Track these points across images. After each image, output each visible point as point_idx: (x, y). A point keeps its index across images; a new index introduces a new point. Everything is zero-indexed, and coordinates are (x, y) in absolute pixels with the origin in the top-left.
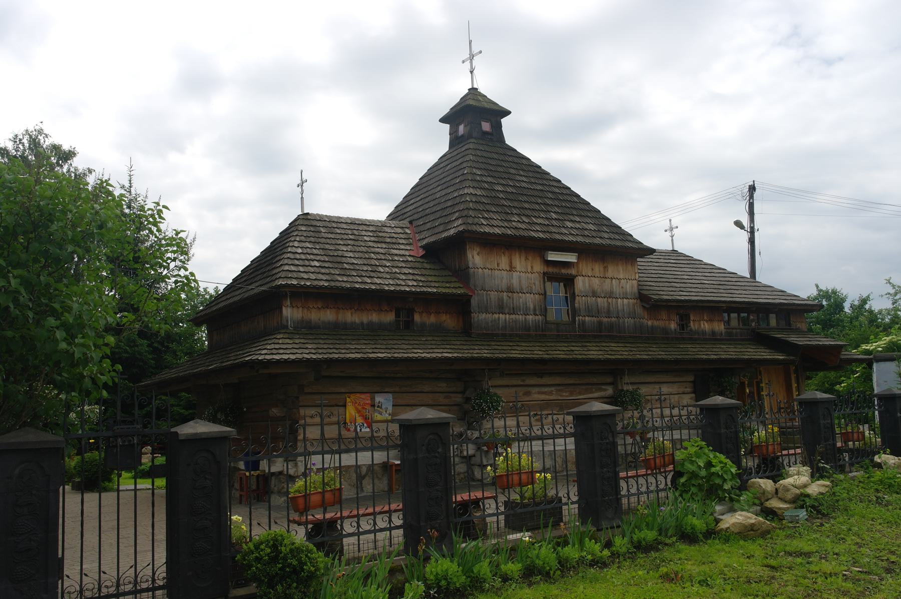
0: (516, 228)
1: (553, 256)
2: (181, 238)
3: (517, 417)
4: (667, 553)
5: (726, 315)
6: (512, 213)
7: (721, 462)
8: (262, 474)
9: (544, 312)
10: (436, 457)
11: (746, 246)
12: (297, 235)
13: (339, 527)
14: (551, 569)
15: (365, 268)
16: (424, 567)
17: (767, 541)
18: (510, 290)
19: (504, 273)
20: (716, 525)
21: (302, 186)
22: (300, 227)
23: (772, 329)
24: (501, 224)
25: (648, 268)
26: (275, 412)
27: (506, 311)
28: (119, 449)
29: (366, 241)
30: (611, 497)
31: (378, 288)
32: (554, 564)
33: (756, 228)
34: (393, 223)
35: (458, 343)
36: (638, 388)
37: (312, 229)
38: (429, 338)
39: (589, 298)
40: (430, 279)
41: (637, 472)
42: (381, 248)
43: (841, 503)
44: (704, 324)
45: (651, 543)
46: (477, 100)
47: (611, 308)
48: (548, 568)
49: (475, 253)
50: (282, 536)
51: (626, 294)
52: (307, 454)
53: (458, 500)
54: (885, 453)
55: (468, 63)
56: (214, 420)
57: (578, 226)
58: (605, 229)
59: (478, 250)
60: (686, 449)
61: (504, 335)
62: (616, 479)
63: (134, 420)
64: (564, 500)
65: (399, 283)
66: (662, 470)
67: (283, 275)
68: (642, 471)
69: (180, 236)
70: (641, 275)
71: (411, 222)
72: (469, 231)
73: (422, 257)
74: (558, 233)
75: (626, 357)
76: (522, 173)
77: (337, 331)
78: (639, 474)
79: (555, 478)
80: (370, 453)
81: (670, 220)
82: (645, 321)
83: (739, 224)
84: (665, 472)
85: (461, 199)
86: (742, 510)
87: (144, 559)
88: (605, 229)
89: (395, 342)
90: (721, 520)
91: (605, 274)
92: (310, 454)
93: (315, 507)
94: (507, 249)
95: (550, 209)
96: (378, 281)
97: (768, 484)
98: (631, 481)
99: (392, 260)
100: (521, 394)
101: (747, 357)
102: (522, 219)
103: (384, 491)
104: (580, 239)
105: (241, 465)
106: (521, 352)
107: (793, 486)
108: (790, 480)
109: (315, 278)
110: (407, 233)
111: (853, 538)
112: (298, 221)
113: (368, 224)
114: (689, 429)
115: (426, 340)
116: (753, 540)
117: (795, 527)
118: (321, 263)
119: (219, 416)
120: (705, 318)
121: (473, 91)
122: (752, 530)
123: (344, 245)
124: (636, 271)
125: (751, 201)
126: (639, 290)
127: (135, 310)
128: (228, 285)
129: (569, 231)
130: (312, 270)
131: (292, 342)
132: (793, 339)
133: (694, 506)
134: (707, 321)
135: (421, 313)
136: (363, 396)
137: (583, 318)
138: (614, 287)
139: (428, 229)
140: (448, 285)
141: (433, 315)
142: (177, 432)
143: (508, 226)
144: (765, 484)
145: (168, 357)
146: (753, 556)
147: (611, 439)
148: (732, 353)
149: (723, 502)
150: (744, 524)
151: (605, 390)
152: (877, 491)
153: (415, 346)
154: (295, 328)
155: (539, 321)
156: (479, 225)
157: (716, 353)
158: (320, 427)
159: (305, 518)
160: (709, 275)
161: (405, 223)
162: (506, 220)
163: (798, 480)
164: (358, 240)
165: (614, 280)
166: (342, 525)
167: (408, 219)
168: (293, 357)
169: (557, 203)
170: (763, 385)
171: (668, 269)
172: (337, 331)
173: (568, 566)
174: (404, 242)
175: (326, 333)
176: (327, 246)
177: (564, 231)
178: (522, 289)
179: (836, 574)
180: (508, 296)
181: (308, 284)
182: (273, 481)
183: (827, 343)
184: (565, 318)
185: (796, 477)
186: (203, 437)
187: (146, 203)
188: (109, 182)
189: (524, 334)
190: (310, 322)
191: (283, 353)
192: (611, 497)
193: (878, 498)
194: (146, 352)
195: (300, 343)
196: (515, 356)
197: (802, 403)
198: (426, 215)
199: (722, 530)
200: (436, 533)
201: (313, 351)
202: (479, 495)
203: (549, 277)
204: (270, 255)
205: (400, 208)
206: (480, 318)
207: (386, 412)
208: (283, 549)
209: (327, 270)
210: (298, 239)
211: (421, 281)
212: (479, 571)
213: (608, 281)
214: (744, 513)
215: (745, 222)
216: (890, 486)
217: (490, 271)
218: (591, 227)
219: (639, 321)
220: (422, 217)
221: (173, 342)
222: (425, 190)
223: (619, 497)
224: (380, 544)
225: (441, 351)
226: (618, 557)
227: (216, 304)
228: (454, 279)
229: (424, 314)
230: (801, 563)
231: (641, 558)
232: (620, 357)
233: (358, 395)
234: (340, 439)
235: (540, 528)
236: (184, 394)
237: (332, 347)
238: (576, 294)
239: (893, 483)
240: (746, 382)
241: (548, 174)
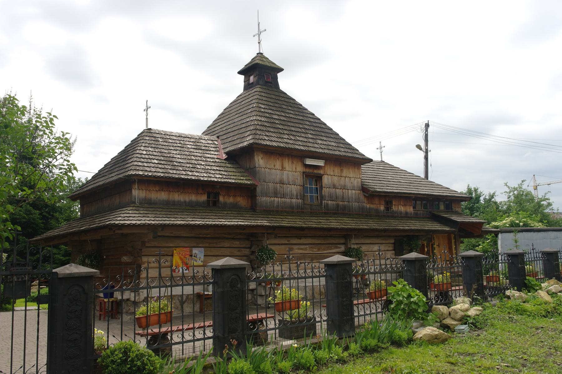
0: (286, 143)
1: (309, 162)
2: (66, 139)
4: (384, 354)
6: (284, 133)
7: (417, 295)
8: (115, 300)
10: (236, 290)
11: (423, 160)
12: (143, 143)
13: (169, 338)
14: (310, 366)
15: (188, 165)
16: (227, 365)
17: (446, 346)
18: (282, 182)
19: (278, 172)
20: (413, 335)
21: (147, 110)
22: (145, 137)
23: (442, 211)
24: (276, 139)
25: (367, 171)
26: (125, 259)
27: (279, 196)
28: (14, 284)
29: (188, 148)
30: (348, 317)
32: (313, 362)
33: (429, 149)
34: (206, 137)
35: (248, 215)
36: (361, 247)
37: (153, 139)
40: (230, 174)
41: (364, 301)
42: (199, 153)
43: (489, 321)
45: (374, 347)
46: (262, 61)
48: (309, 365)
49: (260, 158)
50: (130, 345)
51: (354, 187)
52: (148, 287)
53: (249, 319)
54: (514, 290)
55: (257, 37)
56: (83, 264)
57: (325, 143)
58: (342, 145)
59: (262, 156)
60: (395, 286)
61: (277, 211)
62: (351, 305)
63: (26, 264)
64: (318, 319)
65: (210, 176)
66: (379, 299)
67: (133, 168)
68: (367, 300)
69: (65, 137)
70: (363, 175)
71: (218, 137)
72: (256, 144)
74: (313, 147)
75: (354, 227)
76: (290, 108)
78: (365, 302)
79: (313, 304)
81: (380, 142)
82: (365, 205)
83: (419, 147)
84: (381, 300)
85: (251, 123)
86: (430, 325)
88: (342, 145)
89: (207, 214)
90: (417, 332)
91: (341, 174)
92: (151, 288)
93: (153, 325)
94: (281, 156)
95: (307, 131)
96: (197, 174)
97: (445, 309)
98: (360, 306)
99: (206, 161)
101: (427, 228)
102: (290, 137)
103: (197, 312)
104: (326, 151)
105: (102, 295)
106: (288, 223)
107: (460, 310)
108: (458, 306)
109: (155, 171)
110: (215, 144)
111: (499, 344)
112: (144, 134)
113: (190, 137)
114: (391, 273)
115: (227, 213)
116: (437, 345)
117: (463, 337)
118: (159, 161)
119: (87, 261)
121: (260, 54)
122: (436, 338)
123: (174, 150)
124: (361, 173)
125: (426, 133)
126: (362, 185)
127: (31, 187)
128: (97, 174)
129: (319, 147)
130: (153, 165)
131: (138, 212)
132: (455, 218)
133: (399, 323)
134: (403, 205)
135: (224, 196)
136: (185, 249)
137: (327, 202)
138: (347, 183)
139: (230, 142)
140: (242, 178)
141: (231, 197)
143: (281, 141)
144: (443, 309)
145: (53, 222)
146: (439, 356)
147: (349, 279)
148: (418, 226)
149: (418, 320)
150: (431, 335)
151: (340, 248)
152: (509, 313)
153: (220, 217)
154: (140, 203)
155: (299, 203)
156: (263, 140)
157: (408, 226)
158: (158, 270)
159: (146, 331)
160: (404, 177)
161: (214, 138)
162: (280, 138)
163: (463, 307)
164: (183, 147)
165: (347, 178)
166: (171, 337)
167: (217, 135)
168: (139, 222)
169: (312, 128)
170: (435, 246)
171: (378, 172)
173: (322, 363)
175: (161, 207)
176: (163, 150)
177: (316, 146)
178: (289, 182)
179: (493, 368)
180: (280, 186)
181: (150, 175)
182: (124, 304)
183: (474, 221)
185: (462, 304)
186: (76, 276)
187: (41, 113)
188: (15, 97)
189: (290, 211)
191: (132, 220)
192: (348, 317)
193: (510, 318)
194: (38, 219)
195: (144, 213)
196: (285, 225)
197: (463, 258)
199: (417, 338)
200: (236, 342)
201: (153, 219)
202: (263, 315)
203: (306, 175)
204: (124, 155)
205: (211, 128)
206: (263, 200)
207: (200, 260)
208: (131, 354)
209: (163, 166)
210: (143, 145)
211: (224, 175)
212: (264, 367)
213: (343, 179)
214: (431, 327)
215: (423, 146)
216: (517, 310)
217: (269, 170)
218: (333, 144)
220: (225, 134)
221: (56, 212)
222: (228, 117)
223: (353, 317)
224: (197, 349)
225: (237, 220)
226: (353, 356)
227: (87, 187)
229: (226, 197)
230: (469, 361)
231: (368, 358)
232: (350, 227)
233: (181, 248)
235: (303, 337)
236: (63, 246)
237: (165, 216)
238: (323, 186)
239: (519, 308)
240: (425, 244)
241: (306, 110)
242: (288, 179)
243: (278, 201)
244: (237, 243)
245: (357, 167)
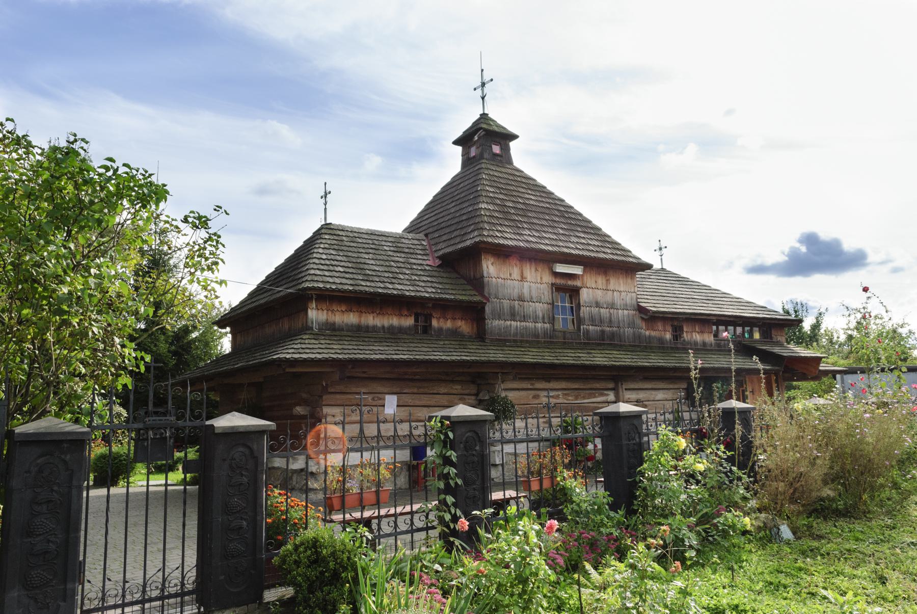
1: (561, 268)
3: (526, 418)
5: (714, 328)
9: (552, 320)
10: (474, 455)
12: (321, 243)
15: (386, 275)
18: (521, 299)
21: (326, 197)
23: (756, 341)
24: (513, 236)
31: (400, 293)
34: (410, 236)
37: (336, 238)
38: (446, 342)
49: (489, 263)
51: (626, 305)
61: (515, 341)
67: (309, 278)
71: (426, 235)
76: (530, 192)
80: (393, 451)
87: (174, 560)
89: (415, 345)
96: (400, 287)
120: (697, 329)
121: (484, 117)
134: (698, 332)
135: (438, 319)
141: (449, 321)
142: (213, 425)
147: (638, 440)
153: (436, 350)
154: (320, 329)
161: (421, 236)
162: (518, 234)
167: (423, 233)
169: (563, 220)
172: (359, 333)
174: (421, 252)
176: (350, 254)
184: (570, 327)
186: (241, 430)
198: (441, 228)
201: (339, 351)
205: (415, 223)
206: (494, 324)
213: (610, 293)
225: (459, 354)
228: (469, 287)
229: (441, 320)
234: (379, 436)
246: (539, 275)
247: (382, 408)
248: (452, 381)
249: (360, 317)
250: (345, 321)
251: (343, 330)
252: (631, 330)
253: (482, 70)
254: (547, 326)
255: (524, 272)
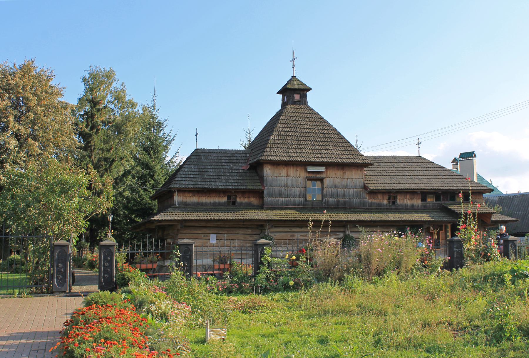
1: (310, 169)
9: (305, 196)
18: (286, 186)
27: (283, 196)
39: (332, 189)
44: (406, 201)
47: (346, 194)
51: (356, 186)
73: (248, 170)
77: (197, 207)
82: (367, 200)
94: (286, 166)
100: (289, 236)
126: (364, 184)
134: (409, 199)
137: (328, 199)
138: (349, 184)
154: (179, 205)
164: (218, 162)
190: (186, 202)
206: (268, 200)
213: (346, 180)
219: (363, 200)
242: (292, 183)
243: (283, 200)
244: (249, 231)
245: (360, 170)
246: (298, 173)
247: (209, 240)
248: (247, 228)
249: (199, 198)
250: (191, 201)
251: (190, 205)
252: (358, 200)
253: (293, 51)
254: (302, 199)
255: (289, 172)
